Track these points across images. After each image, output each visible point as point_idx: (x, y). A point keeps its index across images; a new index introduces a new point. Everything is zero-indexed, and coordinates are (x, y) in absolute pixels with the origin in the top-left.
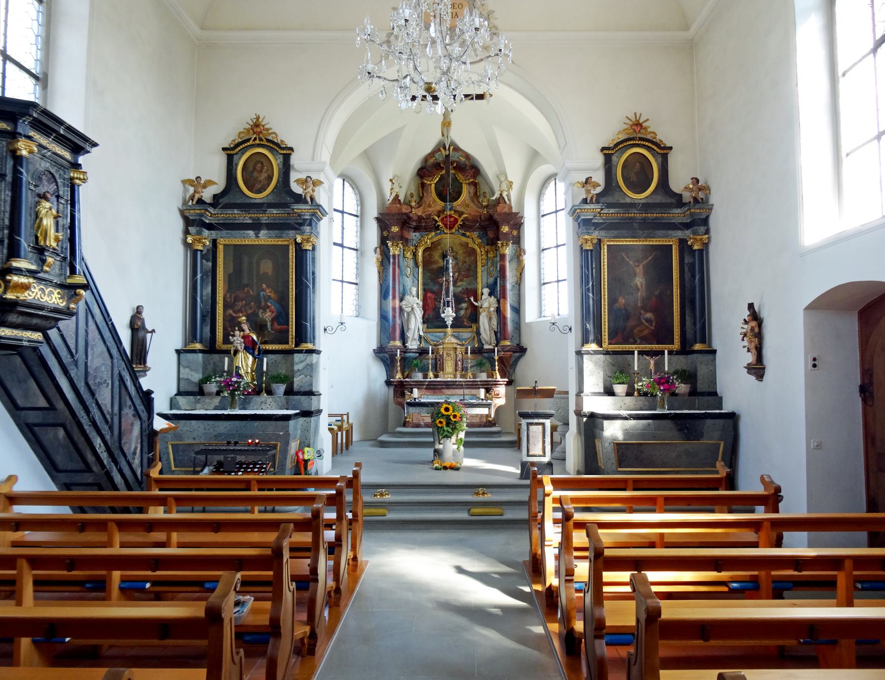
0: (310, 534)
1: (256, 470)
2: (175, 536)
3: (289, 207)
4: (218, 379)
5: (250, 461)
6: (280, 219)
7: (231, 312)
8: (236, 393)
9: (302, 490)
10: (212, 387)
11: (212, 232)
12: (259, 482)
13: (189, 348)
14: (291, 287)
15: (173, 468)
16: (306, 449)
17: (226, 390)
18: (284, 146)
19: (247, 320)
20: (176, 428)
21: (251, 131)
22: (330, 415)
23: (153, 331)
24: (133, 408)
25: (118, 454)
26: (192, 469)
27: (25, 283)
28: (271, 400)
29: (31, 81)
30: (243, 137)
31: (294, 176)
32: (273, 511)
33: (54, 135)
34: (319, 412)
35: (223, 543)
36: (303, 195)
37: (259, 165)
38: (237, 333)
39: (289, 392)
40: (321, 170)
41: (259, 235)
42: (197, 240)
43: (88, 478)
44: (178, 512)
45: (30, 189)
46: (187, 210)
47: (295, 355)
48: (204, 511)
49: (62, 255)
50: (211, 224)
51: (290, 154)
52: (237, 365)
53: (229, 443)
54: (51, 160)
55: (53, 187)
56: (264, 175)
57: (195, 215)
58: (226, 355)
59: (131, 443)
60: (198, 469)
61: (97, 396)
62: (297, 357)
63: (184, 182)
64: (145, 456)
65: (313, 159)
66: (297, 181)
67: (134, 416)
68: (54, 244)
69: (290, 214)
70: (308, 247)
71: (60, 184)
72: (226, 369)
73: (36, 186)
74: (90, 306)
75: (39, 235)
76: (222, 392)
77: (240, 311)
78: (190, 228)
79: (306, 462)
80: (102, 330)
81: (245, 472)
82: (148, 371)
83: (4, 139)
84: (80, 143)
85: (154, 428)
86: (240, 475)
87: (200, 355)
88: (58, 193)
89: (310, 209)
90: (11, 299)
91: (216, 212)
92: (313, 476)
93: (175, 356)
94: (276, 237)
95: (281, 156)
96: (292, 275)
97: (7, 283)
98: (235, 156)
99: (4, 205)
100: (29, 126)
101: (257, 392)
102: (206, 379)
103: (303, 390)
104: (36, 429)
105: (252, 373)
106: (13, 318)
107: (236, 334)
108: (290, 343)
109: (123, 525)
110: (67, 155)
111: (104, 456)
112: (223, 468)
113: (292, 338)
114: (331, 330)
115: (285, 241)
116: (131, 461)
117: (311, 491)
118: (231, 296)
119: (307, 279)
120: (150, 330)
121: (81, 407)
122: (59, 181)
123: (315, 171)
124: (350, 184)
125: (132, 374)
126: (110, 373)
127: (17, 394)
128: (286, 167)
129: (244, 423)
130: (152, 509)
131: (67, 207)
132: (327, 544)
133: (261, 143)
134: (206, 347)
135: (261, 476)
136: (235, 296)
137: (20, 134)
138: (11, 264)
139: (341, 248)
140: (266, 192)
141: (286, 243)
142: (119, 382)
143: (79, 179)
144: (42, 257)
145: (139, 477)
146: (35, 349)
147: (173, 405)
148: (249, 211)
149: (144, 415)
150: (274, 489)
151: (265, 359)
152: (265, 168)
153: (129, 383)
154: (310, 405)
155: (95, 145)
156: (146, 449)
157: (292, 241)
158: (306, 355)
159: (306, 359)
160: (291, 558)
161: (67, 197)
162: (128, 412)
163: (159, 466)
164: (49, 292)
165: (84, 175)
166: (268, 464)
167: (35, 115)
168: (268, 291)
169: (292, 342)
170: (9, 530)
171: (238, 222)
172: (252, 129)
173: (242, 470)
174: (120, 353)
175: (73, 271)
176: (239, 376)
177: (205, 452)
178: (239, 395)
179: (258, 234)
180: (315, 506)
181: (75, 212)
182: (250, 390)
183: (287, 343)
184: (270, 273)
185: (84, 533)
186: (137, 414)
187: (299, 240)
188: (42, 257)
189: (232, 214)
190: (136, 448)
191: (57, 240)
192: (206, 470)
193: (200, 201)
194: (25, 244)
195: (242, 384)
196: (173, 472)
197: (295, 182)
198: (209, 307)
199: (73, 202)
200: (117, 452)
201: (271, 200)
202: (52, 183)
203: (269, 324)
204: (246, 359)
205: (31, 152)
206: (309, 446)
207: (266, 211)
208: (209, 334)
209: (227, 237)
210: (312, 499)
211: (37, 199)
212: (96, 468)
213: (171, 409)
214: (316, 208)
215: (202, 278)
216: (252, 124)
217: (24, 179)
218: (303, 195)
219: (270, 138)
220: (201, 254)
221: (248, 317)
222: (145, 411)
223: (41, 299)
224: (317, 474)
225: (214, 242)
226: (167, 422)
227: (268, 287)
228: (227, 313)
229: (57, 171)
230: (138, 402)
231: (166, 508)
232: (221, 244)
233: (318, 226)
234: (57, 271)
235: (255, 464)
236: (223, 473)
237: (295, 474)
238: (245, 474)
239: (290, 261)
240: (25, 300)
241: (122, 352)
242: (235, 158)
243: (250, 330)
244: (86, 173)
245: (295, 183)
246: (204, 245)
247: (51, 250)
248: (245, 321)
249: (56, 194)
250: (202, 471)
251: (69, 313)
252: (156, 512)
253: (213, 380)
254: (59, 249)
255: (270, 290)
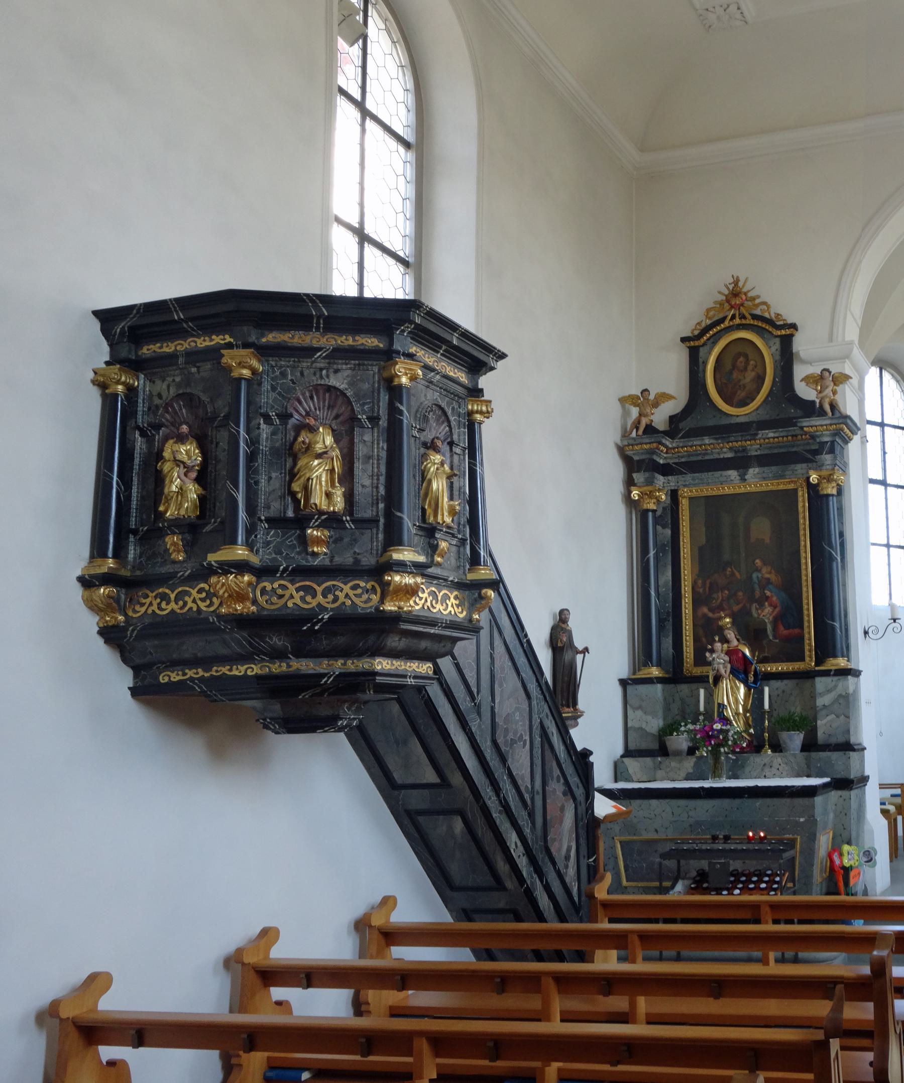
0: (871, 1005)
1: (763, 885)
2: (643, 1004)
3: (795, 425)
4: (690, 727)
5: (752, 870)
6: (780, 447)
7: (705, 610)
8: (722, 750)
9: (843, 922)
10: (680, 741)
11: (670, 478)
12: (774, 906)
13: (640, 675)
14: (803, 561)
15: (625, 883)
16: (846, 848)
17: (705, 746)
18: (781, 323)
19: (733, 623)
20: (628, 813)
21: (726, 305)
22: (882, 786)
23: (586, 650)
24: (562, 780)
25: (543, 861)
26: (657, 884)
27: (410, 585)
28: (779, 760)
29: (397, 270)
30: (714, 316)
31: (800, 372)
32: (796, 960)
33: (444, 347)
34: (864, 780)
35: (721, 1016)
36: (818, 401)
37: (742, 359)
38: (718, 645)
39: (810, 745)
40: (847, 356)
41: (746, 477)
42: (646, 494)
43: (500, 901)
44: (646, 959)
45: (413, 436)
46: (629, 445)
47: (818, 680)
48: (678, 958)
49: (460, 536)
50: (668, 464)
51: (792, 336)
52: (720, 701)
53: (715, 838)
54: (441, 388)
55: (443, 429)
56: (750, 375)
57: (642, 453)
58: (701, 684)
59: (561, 840)
60: (667, 884)
61: (509, 762)
62: (821, 683)
63: (623, 400)
64: (584, 863)
65: (831, 339)
66: (807, 379)
67: (564, 794)
68: (448, 520)
69: (796, 436)
70: (831, 490)
71: (453, 423)
72: (702, 708)
73: (421, 430)
74: (496, 614)
75: (426, 507)
76: (698, 749)
77: (720, 608)
78: (635, 475)
79: (846, 870)
80: (514, 653)
81: (745, 890)
82: (580, 716)
83: (375, 363)
84: (481, 356)
85: (595, 814)
86: (737, 895)
87: (659, 686)
88: (452, 438)
89: (831, 425)
90: (391, 612)
91: (674, 445)
92: (860, 898)
93: (618, 690)
94: (776, 477)
95: (778, 341)
96: (805, 541)
97: (385, 586)
98: (701, 349)
99: (378, 464)
100: (409, 339)
101: (756, 747)
102: (670, 728)
103: (833, 741)
104: (421, 819)
105: (745, 715)
106: (394, 642)
107: (715, 648)
108: (807, 659)
109: (565, 982)
110: (462, 377)
111: (523, 862)
112: (707, 882)
113: (810, 651)
114: (895, 629)
115: (789, 483)
116: (563, 871)
117: (859, 926)
118: (704, 584)
119: (830, 545)
120: (580, 648)
121: (488, 782)
122: (452, 419)
123: (817, 362)
124: (893, 375)
125: (560, 725)
126: (527, 723)
127: (392, 762)
128: (787, 358)
129: (737, 802)
130: (599, 954)
131: (464, 459)
132: (900, 1025)
133: (744, 322)
134: (667, 672)
135: (773, 897)
136: (711, 584)
137: (398, 352)
138: (391, 555)
139: (883, 488)
140: (755, 402)
141: (792, 486)
142: (541, 737)
143: (481, 413)
144: (432, 541)
145: (576, 899)
146: (420, 689)
147: (618, 774)
148: (729, 437)
149: (579, 792)
150: (796, 920)
151: (766, 689)
152: (752, 362)
153: (556, 739)
154: (848, 768)
155: (502, 356)
156: (584, 851)
157: (802, 481)
158: (835, 678)
159: (836, 687)
160: (843, 1048)
161: (464, 442)
162: (556, 787)
163: (609, 878)
164: (442, 596)
165: (487, 406)
166: (784, 875)
167: (418, 320)
168: (764, 570)
169: (810, 657)
170: (393, 989)
171: (711, 457)
172: (728, 301)
173: (740, 886)
174: (541, 689)
175: (475, 560)
176: (725, 720)
177: (678, 854)
178: (727, 753)
179: (745, 474)
180: (875, 953)
181: (476, 465)
182: (744, 745)
183: (802, 659)
184: (767, 541)
185: (504, 995)
186: (569, 791)
187: (814, 478)
188: (432, 541)
189: (700, 446)
190: (569, 850)
191: (452, 512)
192: (679, 887)
193: (650, 430)
194: (409, 523)
195: (730, 734)
196: (624, 890)
197: (802, 380)
198: (669, 605)
199: (473, 449)
200: (541, 856)
201: (764, 415)
202: (443, 422)
203: (769, 628)
204: (735, 689)
205: (413, 378)
206: (849, 843)
207: (757, 434)
208: (671, 650)
209: (695, 485)
210: (870, 940)
211: (422, 450)
212: (510, 884)
213: (616, 781)
214: (841, 421)
215: (656, 556)
216: (726, 292)
217: (405, 421)
218: (818, 401)
219: (758, 312)
220: (654, 517)
221: (733, 616)
222: (580, 785)
223: (431, 609)
224: (867, 895)
225: (674, 495)
226: (613, 803)
227: (765, 564)
228: (700, 613)
229: (448, 404)
230: (569, 770)
231: (623, 952)
232: (685, 497)
233: (845, 451)
234: (453, 561)
235: (760, 875)
236: (707, 891)
237: (828, 893)
238: (744, 894)
239: (801, 516)
240: (410, 612)
241: (544, 687)
242: (702, 352)
243: (738, 640)
244: (490, 402)
245: (803, 383)
246: (658, 501)
247: (444, 530)
248: (729, 626)
249: (449, 440)
250: (673, 887)
251: (472, 628)
252: (606, 960)
253: (683, 729)
254: (456, 527)
255: (769, 569)
